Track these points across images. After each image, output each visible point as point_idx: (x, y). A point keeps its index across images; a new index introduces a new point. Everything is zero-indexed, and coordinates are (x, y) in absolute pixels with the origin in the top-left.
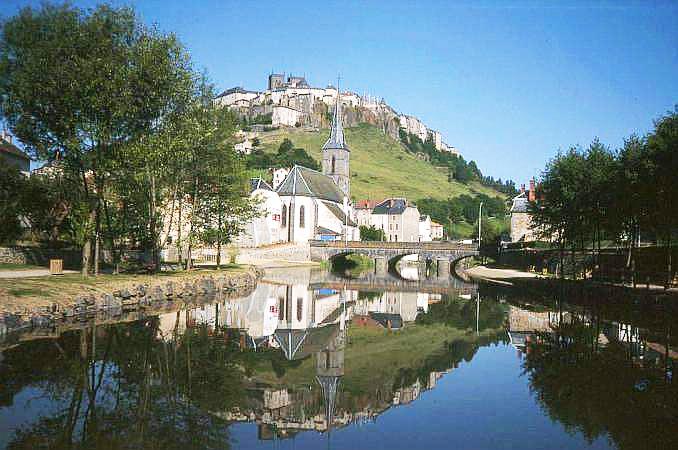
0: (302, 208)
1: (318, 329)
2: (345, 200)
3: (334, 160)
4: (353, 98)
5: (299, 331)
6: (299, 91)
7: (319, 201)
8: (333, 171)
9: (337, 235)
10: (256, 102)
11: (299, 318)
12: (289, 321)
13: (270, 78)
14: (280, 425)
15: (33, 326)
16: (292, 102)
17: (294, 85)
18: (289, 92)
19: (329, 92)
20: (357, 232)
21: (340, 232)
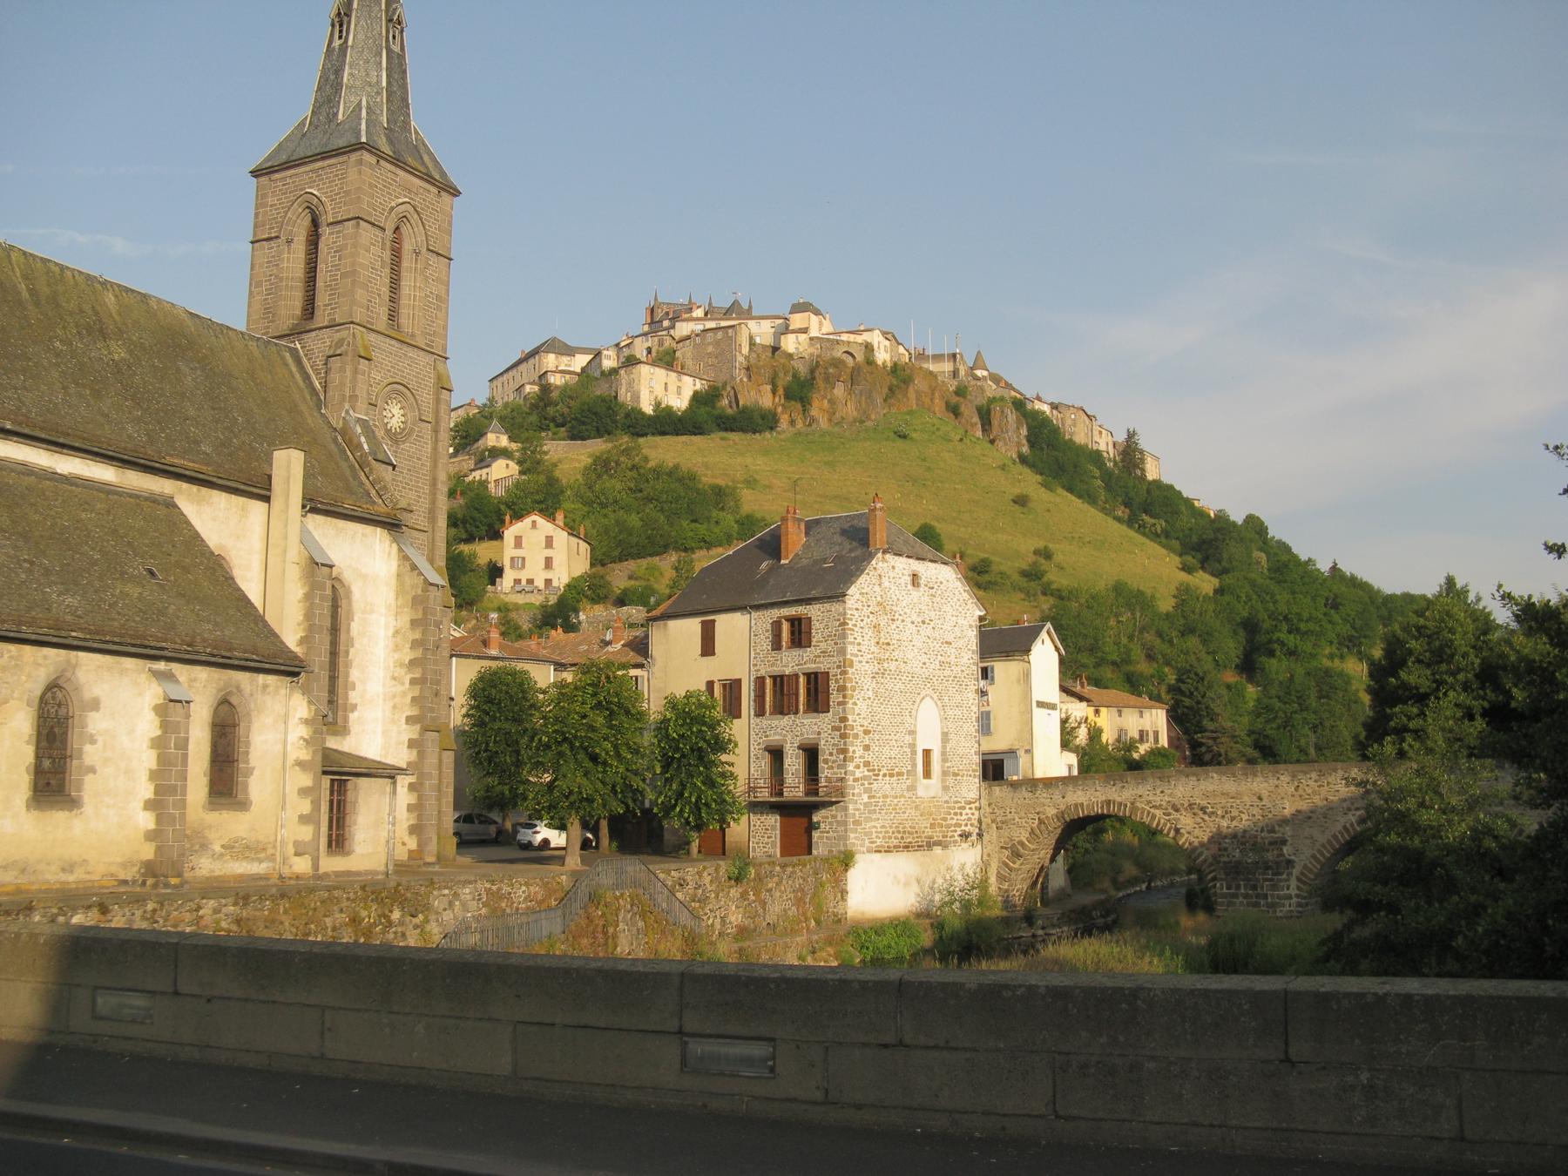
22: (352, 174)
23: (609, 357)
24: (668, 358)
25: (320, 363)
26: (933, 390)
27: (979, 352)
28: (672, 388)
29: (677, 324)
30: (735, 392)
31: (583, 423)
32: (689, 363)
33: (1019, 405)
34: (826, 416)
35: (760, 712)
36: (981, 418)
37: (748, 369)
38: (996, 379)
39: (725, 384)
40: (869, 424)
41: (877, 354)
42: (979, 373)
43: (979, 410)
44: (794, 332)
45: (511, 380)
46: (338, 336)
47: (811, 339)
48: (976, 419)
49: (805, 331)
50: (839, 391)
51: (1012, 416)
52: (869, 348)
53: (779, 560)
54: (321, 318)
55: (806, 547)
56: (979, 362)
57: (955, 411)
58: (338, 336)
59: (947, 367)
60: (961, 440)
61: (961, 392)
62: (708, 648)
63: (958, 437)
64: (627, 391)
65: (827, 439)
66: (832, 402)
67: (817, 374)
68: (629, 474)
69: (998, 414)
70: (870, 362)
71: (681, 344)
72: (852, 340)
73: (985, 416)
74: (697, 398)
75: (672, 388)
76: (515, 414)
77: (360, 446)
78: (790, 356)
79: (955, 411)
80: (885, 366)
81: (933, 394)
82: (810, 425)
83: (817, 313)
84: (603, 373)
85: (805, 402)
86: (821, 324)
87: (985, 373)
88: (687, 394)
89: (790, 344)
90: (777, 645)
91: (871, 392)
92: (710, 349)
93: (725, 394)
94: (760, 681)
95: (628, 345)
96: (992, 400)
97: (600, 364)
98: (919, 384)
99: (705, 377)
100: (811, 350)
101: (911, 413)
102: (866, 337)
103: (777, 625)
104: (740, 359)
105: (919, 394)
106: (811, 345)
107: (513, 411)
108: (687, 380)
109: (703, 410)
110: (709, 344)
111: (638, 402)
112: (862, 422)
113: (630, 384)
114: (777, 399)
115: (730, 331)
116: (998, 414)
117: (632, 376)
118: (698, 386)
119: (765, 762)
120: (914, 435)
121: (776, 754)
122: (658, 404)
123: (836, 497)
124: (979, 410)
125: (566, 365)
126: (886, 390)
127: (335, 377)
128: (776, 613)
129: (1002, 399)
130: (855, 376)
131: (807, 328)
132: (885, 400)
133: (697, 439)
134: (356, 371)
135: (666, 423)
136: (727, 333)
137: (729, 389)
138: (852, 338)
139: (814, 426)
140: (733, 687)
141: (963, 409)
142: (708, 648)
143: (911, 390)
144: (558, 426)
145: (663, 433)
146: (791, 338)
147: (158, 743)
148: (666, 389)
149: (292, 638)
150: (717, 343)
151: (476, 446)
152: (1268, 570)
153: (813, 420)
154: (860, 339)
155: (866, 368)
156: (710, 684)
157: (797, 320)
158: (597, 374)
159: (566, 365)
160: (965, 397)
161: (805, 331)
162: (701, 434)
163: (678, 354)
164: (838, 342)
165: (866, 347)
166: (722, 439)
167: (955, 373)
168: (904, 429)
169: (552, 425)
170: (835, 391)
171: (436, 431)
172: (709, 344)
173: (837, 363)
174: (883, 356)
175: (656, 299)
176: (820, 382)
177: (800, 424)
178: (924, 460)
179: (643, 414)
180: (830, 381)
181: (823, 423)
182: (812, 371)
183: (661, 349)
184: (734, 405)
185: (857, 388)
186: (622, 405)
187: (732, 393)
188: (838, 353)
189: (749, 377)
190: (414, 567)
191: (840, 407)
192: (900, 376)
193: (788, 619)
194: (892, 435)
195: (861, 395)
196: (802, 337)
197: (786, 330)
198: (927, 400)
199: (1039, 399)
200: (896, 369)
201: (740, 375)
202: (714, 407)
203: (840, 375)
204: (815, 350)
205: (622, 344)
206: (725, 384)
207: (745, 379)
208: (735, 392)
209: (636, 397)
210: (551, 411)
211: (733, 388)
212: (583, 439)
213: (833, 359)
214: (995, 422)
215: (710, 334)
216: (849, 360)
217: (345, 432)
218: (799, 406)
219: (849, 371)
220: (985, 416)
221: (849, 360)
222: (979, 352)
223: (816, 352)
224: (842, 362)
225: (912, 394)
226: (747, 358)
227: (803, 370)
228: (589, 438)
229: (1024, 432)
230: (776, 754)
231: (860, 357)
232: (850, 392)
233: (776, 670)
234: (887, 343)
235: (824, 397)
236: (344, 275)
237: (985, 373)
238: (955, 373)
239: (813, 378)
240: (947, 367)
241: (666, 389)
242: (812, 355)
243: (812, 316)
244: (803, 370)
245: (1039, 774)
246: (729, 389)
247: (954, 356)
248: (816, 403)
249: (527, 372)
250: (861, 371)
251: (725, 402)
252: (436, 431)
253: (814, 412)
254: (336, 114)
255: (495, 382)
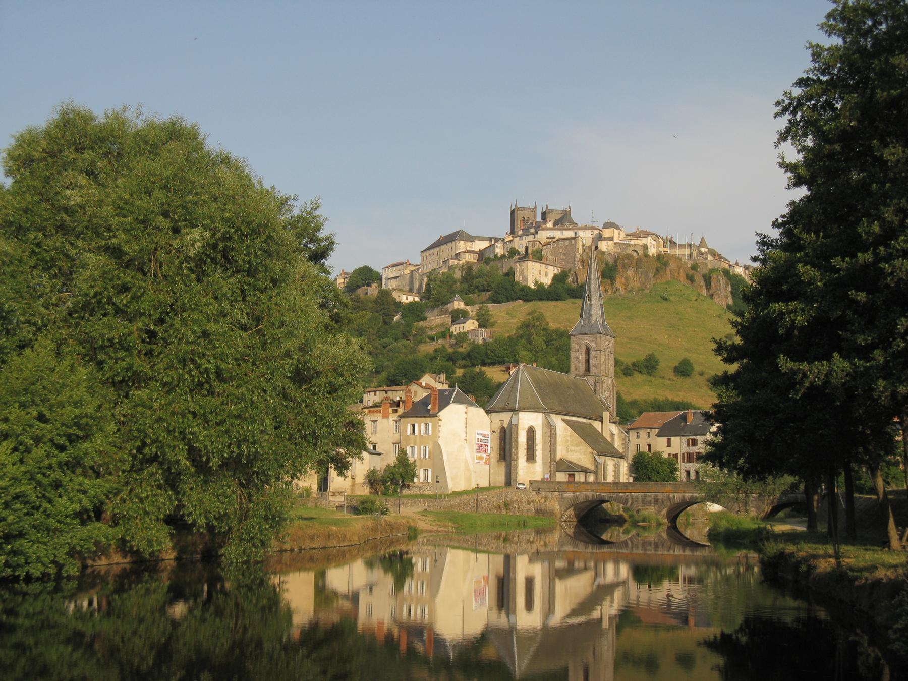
23: (499, 247)
24: (538, 255)
25: (593, 384)
27: (703, 238)
28: (543, 273)
29: (539, 232)
31: (499, 294)
32: (550, 257)
33: (726, 273)
34: (623, 287)
35: (684, 462)
36: (705, 281)
37: (582, 262)
38: (713, 253)
39: (570, 270)
40: (647, 291)
41: (649, 250)
42: (703, 250)
43: (704, 276)
44: (605, 239)
45: (436, 254)
47: (615, 243)
48: (703, 283)
49: (611, 239)
50: (630, 272)
51: (723, 280)
52: (645, 247)
54: (592, 372)
55: (693, 420)
56: (703, 243)
57: (691, 279)
59: (687, 251)
60: (696, 300)
61: (694, 268)
62: (669, 445)
63: (694, 298)
65: (626, 302)
66: (627, 279)
67: (618, 264)
68: (543, 333)
69: (715, 280)
70: (646, 255)
73: (708, 280)
74: (555, 278)
75: (543, 273)
76: (449, 280)
78: (603, 253)
79: (691, 279)
80: (653, 257)
81: (679, 270)
82: (615, 292)
83: (618, 228)
84: (496, 256)
85: (612, 279)
86: (619, 234)
87: (706, 250)
88: (551, 276)
89: (603, 246)
90: (688, 445)
91: (647, 272)
92: (561, 250)
93: (570, 275)
94: (684, 454)
96: (712, 271)
97: (494, 251)
98: (672, 265)
100: (614, 250)
101: (668, 283)
102: (644, 241)
103: (688, 441)
104: (578, 256)
105: (671, 271)
106: (615, 247)
107: (447, 278)
108: (550, 268)
109: (560, 285)
111: (527, 282)
112: (643, 290)
113: (522, 273)
115: (573, 241)
116: (715, 280)
118: (556, 272)
119: (685, 474)
120: (671, 298)
121: (688, 472)
122: (536, 283)
123: (636, 339)
124: (704, 276)
126: (654, 270)
128: (688, 438)
129: (717, 270)
130: (638, 263)
132: (654, 276)
133: (559, 303)
135: (542, 294)
137: (572, 272)
139: (618, 293)
140: (676, 456)
141: (696, 278)
142: (669, 445)
143: (668, 269)
144: (480, 291)
145: (541, 300)
146: (604, 243)
147: (614, 471)
148: (540, 274)
149: (621, 451)
150: (566, 247)
151: (446, 306)
153: (617, 289)
154: (641, 243)
155: (645, 259)
156: (670, 454)
157: (607, 233)
158: (492, 256)
160: (696, 271)
161: (611, 239)
162: (560, 300)
163: (544, 252)
164: (629, 245)
166: (573, 303)
167: (691, 255)
168: (666, 295)
169: (476, 290)
173: (629, 257)
174: (652, 251)
175: (516, 205)
176: (620, 268)
177: (610, 292)
178: (678, 314)
179: (529, 288)
180: (625, 267)
181: (622, 291)
182: (616, 262)
183: (534, 249)
184: (575, 282)
185: (640, 271)
186: (517, 284)
187: (574, 275)
188: (629, 251)
189: (583, 266)
192: (662, 261)
193: (692, 440)
194: (659, 298)
196: (610, 243)
197: (600, 237)
198: (676, 274)
199: (737, 264)
200: (659, 257)
201: (578, 265)
202: (565, 283)
203: (631, 264)
204: (617, 250)
205: (506, 240)
206: (570, 270)
209: (525, 279)
210: (475, 282)
212: (499, 302)
213: (627, 254)
214: (713, 284)
215: (561, 242)
216: (635, 254)
217: (601, 400)
218: (609, 282)
219: (635, 261)
220: (708, 280)
221: (635, 254)
222: (703, 238)
223: (618, 251)
224: (631, 256)
225: (668, 272)
226: (581, 255)
227: (611, 261)
228: (503, 302)
229: (729, 289)
230: (688, 472)
231: (641, 253)
232: (636, 272)
233: (688, 451)
234: (655, 243)
235: (622, 276)
237: (706, 250)
238: (691, 255)
239: (616, 266)
240: (687, 251)
241: (540, 274)
243: (615, 230)
244: (611, 261)
246: (572, 272)
247: (690, 245)
248: (618, 280)
249: (446, 251)
250: (641, 261)
251: (570, 280)
253: (617, 285)
255: (425, 253)
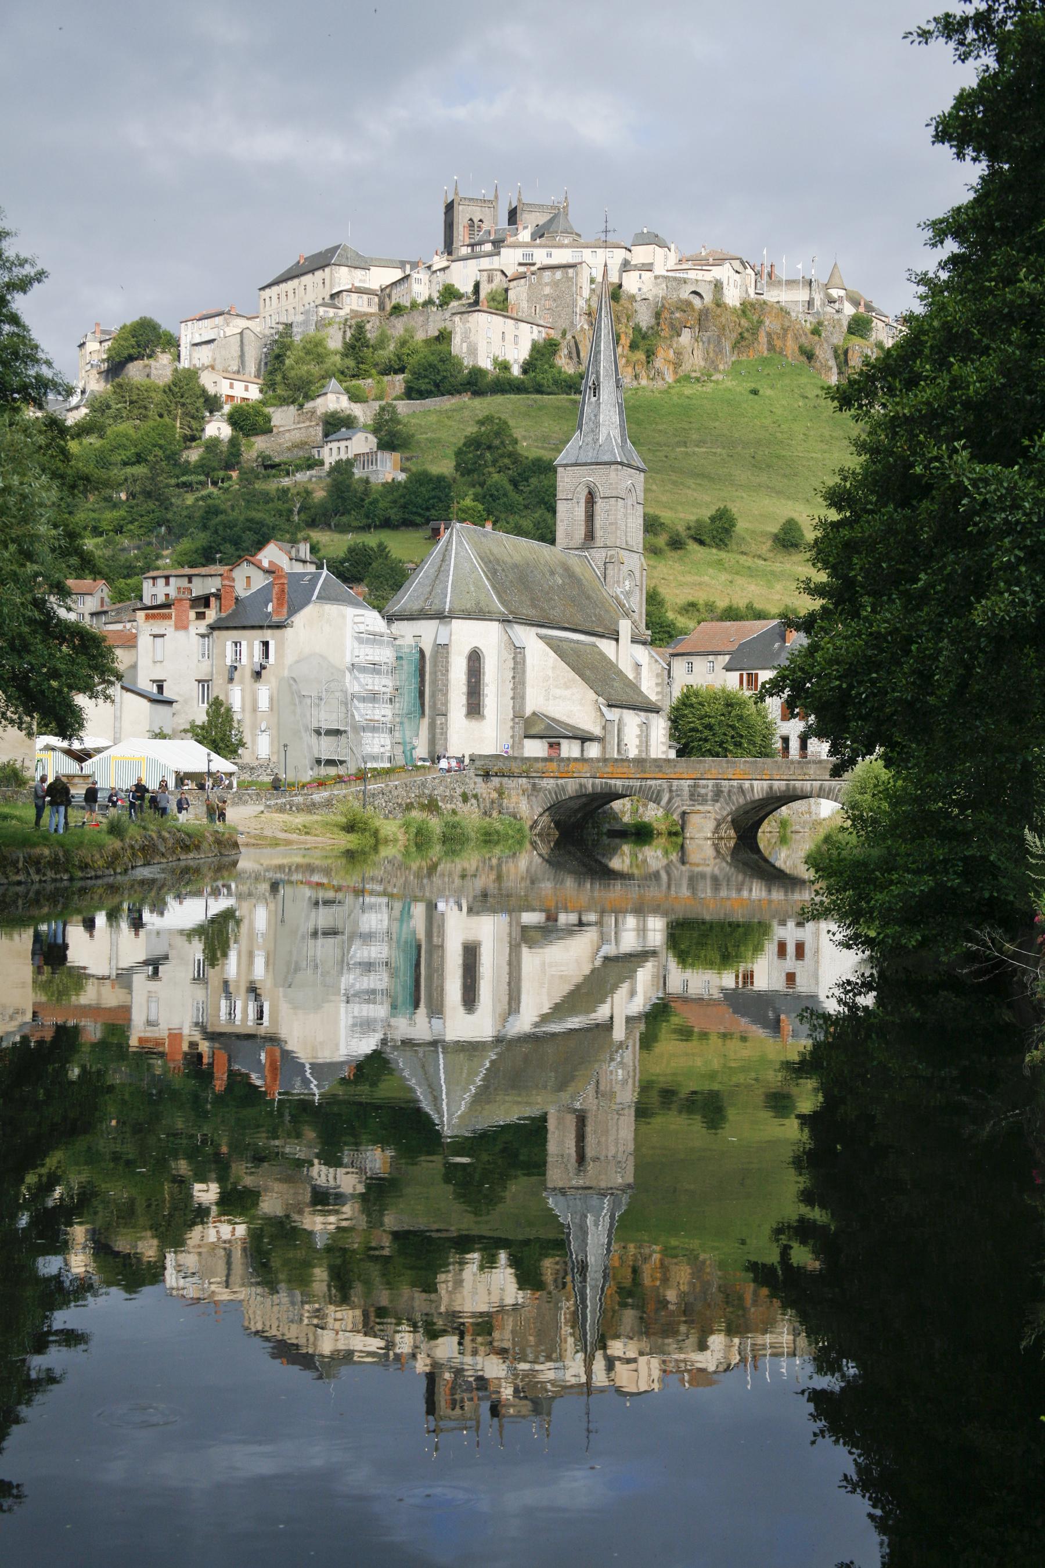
0: (475, 659)
1: (532, 1039)
2: (625, 627)
3: (591, 499)
4: (723, 273)
5: (470, 1048)
6: (540, 256)
7: (528, 637)
8: (590, 535)
9: (585, 739)
10: (399, 297)
11: (470, 999)
12: (436, 1010)
13: (450, 208)
14: (494, 1368)
15: (744, 1069)
16: (518, 294)
17: (525, 236)
18: (510, 259)
19: (641, 254)
20: (660, 727)
21: (597, 731)
22: (613, 475)
26: (785, 330)
29: (503, 250)
30: (576, 343)
34: (671, 368)
46: (610, 553)
47: (656, 277)
48: (832, 363)
49: (648, 267)
50: (686, 338)
53: (785, 642)
54: (599, 542)
58: (610, 553)
64: (463, 341)
70: (719, 304)
71: (514, 283)
72: (700, 278)
75: (509, 337)
77: (624, 605)
83: (663, 245)
92: (547, 290)
95: (444, 269)
99: (541, 322)
100: (654, 291)
110: (547, 284)
114: (619, 350)
115: (571, 271)
117: (468, 325)
118: (535, 336)
125: (360, 281)
127: (610, 572)
130: (703, 318)
131: (652, 264)
134: (619, 570)
136: (567, 273)
138: (699, 275)
141: (818, 352)
148: (503, 339)
149: (653, 698)
150: (556, 284)
152: (368, 1331)
153: (659, 373)
159: (360, 281)
165: (716, 285)
170: (681, 339)
171: (641, 590)
172: (547, 284)
173: (685, 306)
174: (732, 297)
175: (456, 194)
187: (573, 341)
188: (685, 294)
190: (656, 661)
191: (686, 356)
195: (709, 342)
196: (646, 275)
203: (687, 321)
204: (661, 291)
207: (586, 327)
208: (576, 343)
209: (473, 351)
211: (574, 337)
213: (680, 300)
216: (697, 302)
219: (696, 315)
221: (697, 302)
224: (689, 304)
231: (708, 298)
235: (670, 346)
236: (611, 524)
237: (842, 293)
241: (503, 339)
242: (656, 296)
245: (526, 755)
246: (569, 337)
252: (641, 590)
253: (659, 363)
254: (598, 439)
